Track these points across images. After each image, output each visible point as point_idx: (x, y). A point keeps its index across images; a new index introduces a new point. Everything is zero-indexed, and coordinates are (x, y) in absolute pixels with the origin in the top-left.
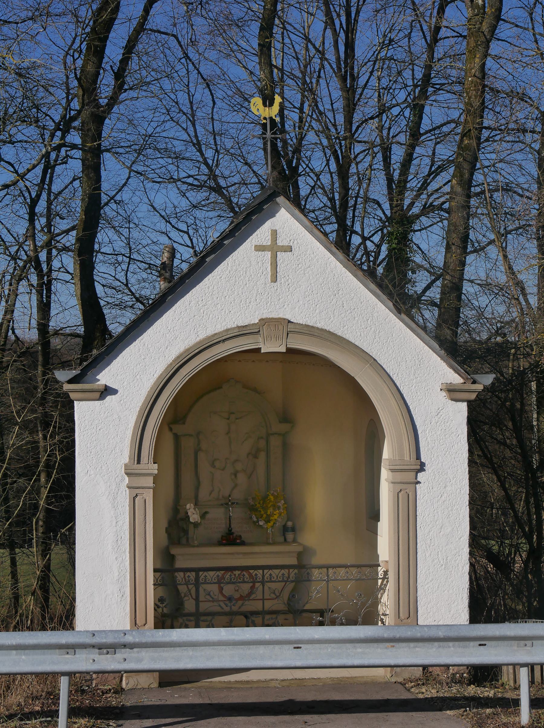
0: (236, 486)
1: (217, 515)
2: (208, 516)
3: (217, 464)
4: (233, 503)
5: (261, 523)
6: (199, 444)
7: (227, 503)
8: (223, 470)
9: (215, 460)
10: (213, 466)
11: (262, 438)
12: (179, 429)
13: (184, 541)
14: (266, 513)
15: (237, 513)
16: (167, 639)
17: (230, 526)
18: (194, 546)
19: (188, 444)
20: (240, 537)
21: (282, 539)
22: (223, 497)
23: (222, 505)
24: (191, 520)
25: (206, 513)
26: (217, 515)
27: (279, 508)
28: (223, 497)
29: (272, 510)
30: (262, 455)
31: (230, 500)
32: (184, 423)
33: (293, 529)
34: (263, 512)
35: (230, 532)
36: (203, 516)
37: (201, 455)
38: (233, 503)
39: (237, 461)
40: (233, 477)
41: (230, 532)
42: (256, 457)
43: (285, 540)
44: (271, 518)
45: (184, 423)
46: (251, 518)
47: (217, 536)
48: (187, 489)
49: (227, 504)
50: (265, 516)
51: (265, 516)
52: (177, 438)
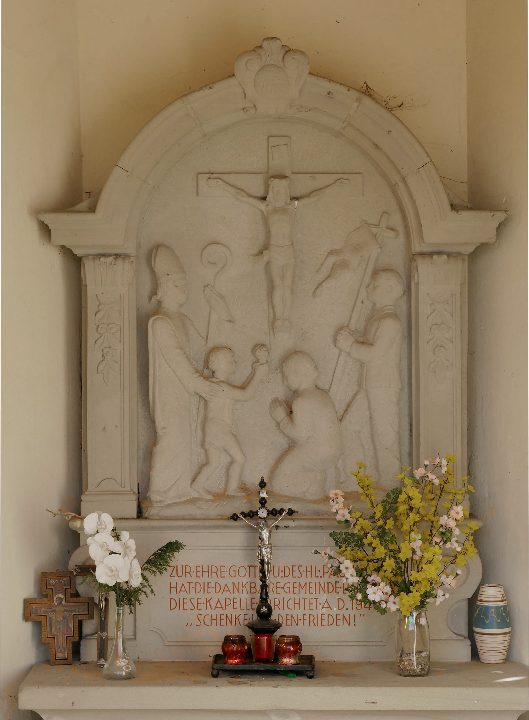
0: (291, 446)
1: (217, 555)
2: (179, 559)
3: (221, 364)
4: (274, 513)
5: (374, 594)
6: (154, 292)
7: (260, 511)
8: (243, 387)
9: (215, 349)
10: (207, 373)
11: (388, 270)
12: (73, 228)
13: (90, 650)
14: (394, 553)
15: (294, 549)
16: (485, 632)
17: (264, 600)
18: (114, 679)
19: (112, 288)
20: (296, 642)
21: (461, 652)
22: (243, 488)
23: (235, 517)
24: (102, 576)
25: (173, 547)
26: (217, 555)
27: (446, 535)
28: (243, 488)
29: (417, 544)
30: (390, 332)
31: (263, 502)
32: (92, 209)
33: (506, 617)
34: (381, 552)
35: (264, 622)
36: (159, 559)
37: (160, 332)
38: (274, 513)
39: (293, 353)
40: (281, 413)
41: (264, 622)
42: (364, 340)
43: (475, 654)
44: (414, 576)
45: (92, 209)
46: (337, 571)
47: (211, 639)
48: (110, 459)
49: (252, 515)
50: (390, 564)
51: (390, 564)
52: (74, 262)
